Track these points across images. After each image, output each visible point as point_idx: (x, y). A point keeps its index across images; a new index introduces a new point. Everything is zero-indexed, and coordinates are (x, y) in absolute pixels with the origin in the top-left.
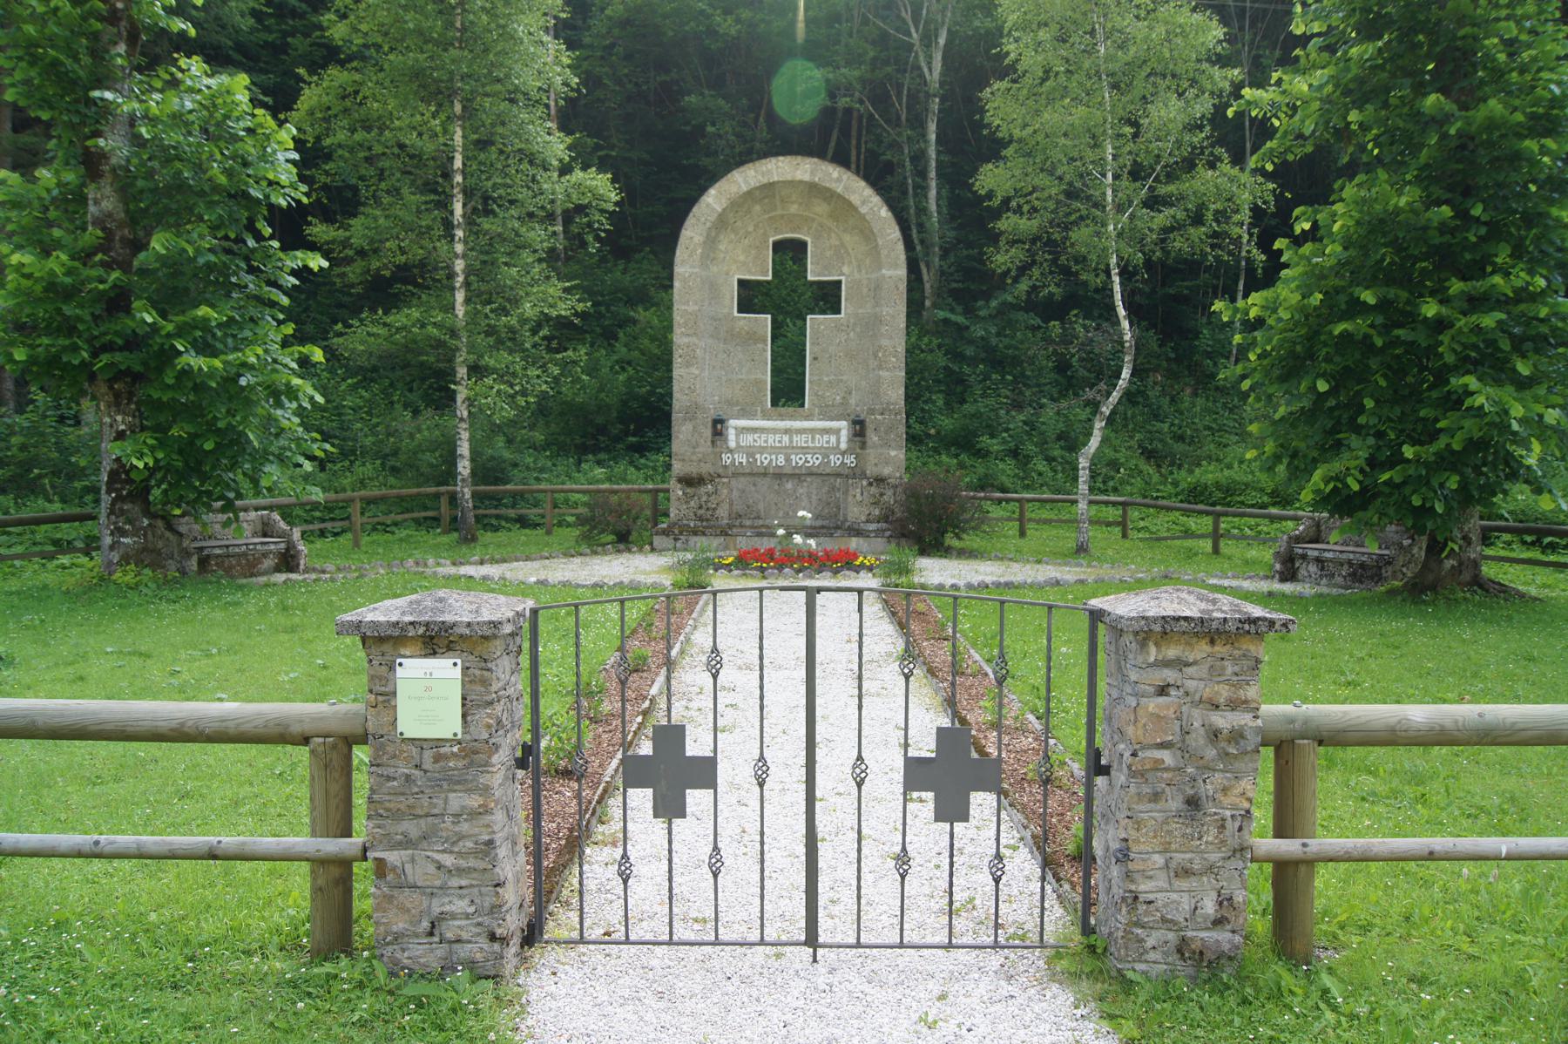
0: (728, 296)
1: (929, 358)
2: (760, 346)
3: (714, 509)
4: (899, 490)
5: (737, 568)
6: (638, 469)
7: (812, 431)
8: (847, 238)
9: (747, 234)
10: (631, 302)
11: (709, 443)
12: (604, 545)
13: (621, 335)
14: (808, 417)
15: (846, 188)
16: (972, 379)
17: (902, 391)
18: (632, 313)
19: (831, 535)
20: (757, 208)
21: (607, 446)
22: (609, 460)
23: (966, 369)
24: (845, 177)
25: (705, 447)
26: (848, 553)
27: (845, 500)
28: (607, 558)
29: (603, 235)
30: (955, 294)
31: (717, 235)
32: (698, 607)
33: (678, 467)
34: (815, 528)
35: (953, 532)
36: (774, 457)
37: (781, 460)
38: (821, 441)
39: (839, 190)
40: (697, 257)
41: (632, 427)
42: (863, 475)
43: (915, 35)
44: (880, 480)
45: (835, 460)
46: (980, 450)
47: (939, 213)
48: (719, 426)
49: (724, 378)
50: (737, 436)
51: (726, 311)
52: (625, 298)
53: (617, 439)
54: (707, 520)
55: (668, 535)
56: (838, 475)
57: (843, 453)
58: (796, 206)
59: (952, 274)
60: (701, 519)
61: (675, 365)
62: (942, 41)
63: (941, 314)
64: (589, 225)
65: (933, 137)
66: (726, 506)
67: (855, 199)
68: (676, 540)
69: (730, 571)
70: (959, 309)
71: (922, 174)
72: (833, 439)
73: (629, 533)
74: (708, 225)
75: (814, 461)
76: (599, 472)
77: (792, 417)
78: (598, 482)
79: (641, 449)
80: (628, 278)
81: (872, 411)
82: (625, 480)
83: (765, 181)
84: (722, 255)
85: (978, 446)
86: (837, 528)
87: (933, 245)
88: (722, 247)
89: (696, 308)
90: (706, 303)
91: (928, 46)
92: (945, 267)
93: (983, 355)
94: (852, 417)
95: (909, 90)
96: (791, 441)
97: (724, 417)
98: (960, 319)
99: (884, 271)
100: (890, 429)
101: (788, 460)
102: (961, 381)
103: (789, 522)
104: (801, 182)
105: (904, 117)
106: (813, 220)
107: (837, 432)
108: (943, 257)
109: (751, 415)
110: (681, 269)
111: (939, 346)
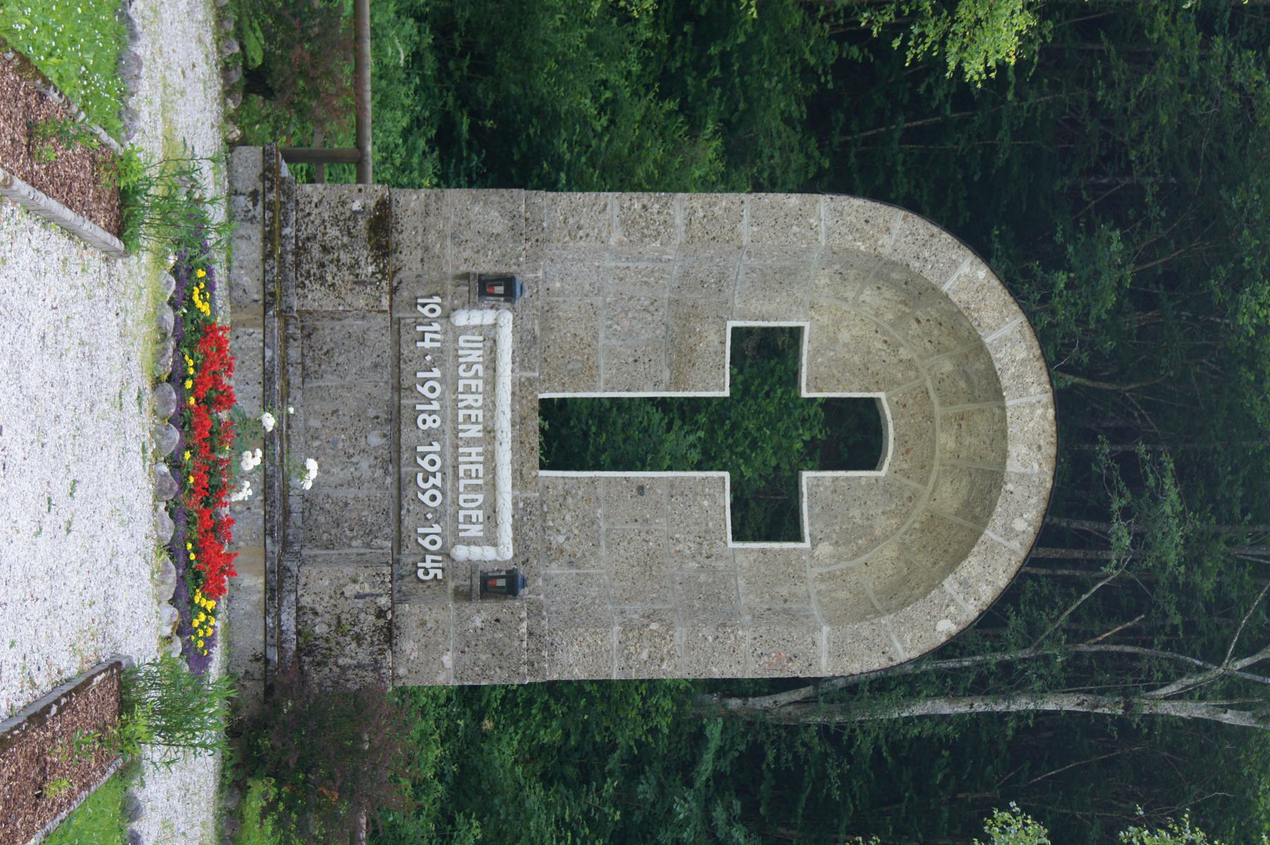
0: (769, 308)
1: (632, 714)
2: (666, 375)
3: (322, 279)
4: (370, 677)
5: (179, 322)
6: (406, 133)
7: (492, 486)
8: (889, 551)
9: (893, 346)
10: (727, 127)
11: (463, 268)
12: (239, 35)
13: (670, 105)
14: (519, 477)
15: (992, 548)
16: (593, 799)
17: (579, 674)
18: (711, 127)
19: (269, 532)
20: (948, 367)
21: (450, 75)
22: (423, 78)
23: (610, 786)
24: (1015, 544)
25: (455, 260)
26: (225, 567)
27: (346, 559)
28: (209, 38)
29: (896, 44)
30: (756, 752)
31: (894, 285)
32: (54, 205)
33: (411, 202)
34: (285, 496)
35: (279, 798)
36: (436, 406)
37: (429, 423)
38: (471, 505)
39: (988, 533)
40: (849, 241)
41: (489, 124)
42: (399, 597)
43: (1239, 665)
44: (389, 634)
45: (431, 535)
46: (451, 821)
47: (908, 720)
48: (500, 289)
49: (598, 301)
50: (480, 329)
51: (738, 304)
52: (734, 119)
53: (464, 99)
54: (298, 265)
55: (263, 177)
56: (399, 543)
57: (445, 553)
58: (951, 444)
59: (791, 747)
60: (300, 250)
61: (626, 196)
62: (1229, 717)
63: (714, 732)
64: (916, 15)
65: (1050, 706)
66: (329, 304)
67: (971, 566)
68: (254, 195)
69: (173, 304)
70: (725, 765)
71: (980, 688)
72: (475, 531)
73: (268, 93)
74: (916, 265)
75: (428, 493)
76: (399, 53)
77: (519, 443)
78: (378, 49)
79: (444, 142)
80: (776, 124)
81: (536, 611)
82: (382, 105)
83: (1005, 381)
84: (850, 295)
85: (460, 818)
86: (286, 544)
87: (846, 711)
88: (868, 295)
89: (746, 240)
90: (755, 263)
91: (1228, 694)
92: (805, 736)
93: (637, 817)
94: (522, 571)
95: (1134, 657)
96: (470, 442)
97: (519, 303)
98: (706, 766)
99: (826, 629)
100: (497, 650)
101: (430, 436)
102: (587, 776)
103: (298, 440)
104: (1004, 455)
105: (1083, 647)
106: (924, 481)
107: (491, 539)
108: (824, 730)
109: (522, 358)
110: (824, 204)
111: (654, 731)
